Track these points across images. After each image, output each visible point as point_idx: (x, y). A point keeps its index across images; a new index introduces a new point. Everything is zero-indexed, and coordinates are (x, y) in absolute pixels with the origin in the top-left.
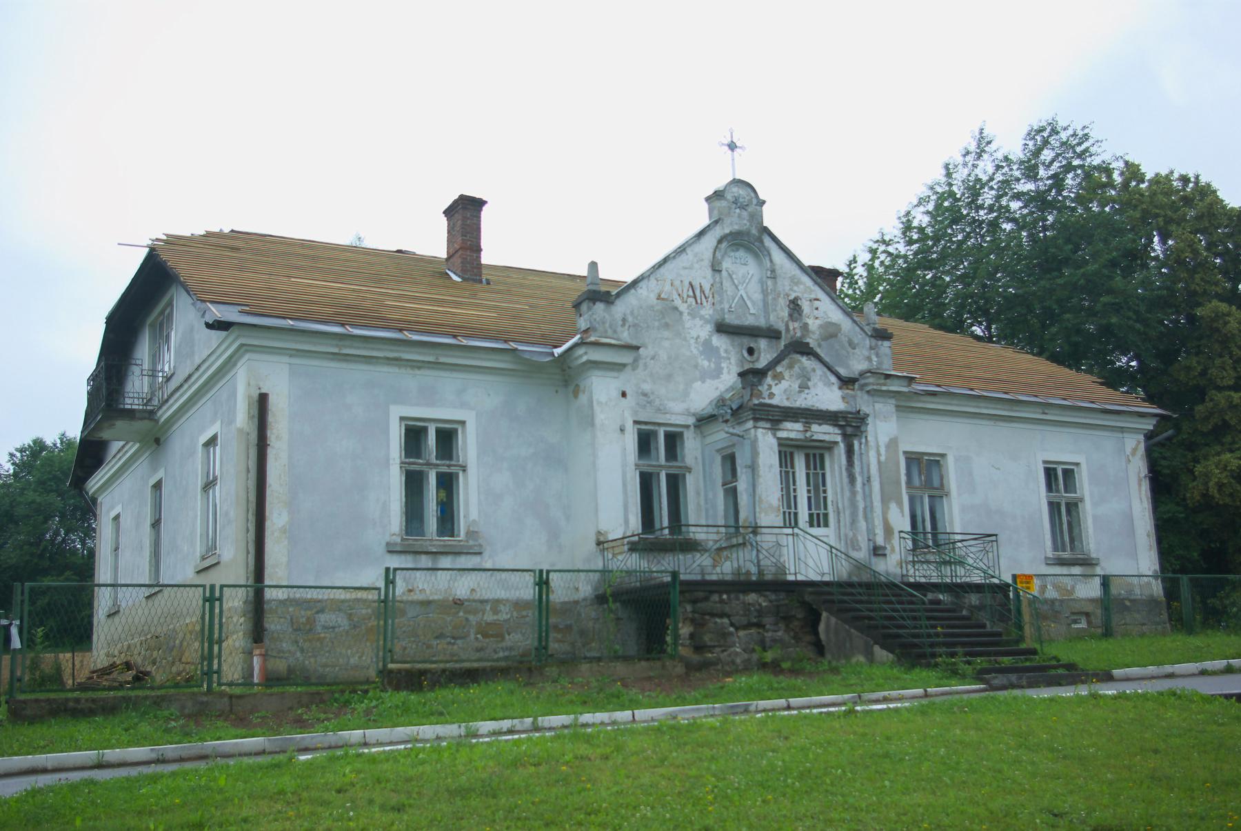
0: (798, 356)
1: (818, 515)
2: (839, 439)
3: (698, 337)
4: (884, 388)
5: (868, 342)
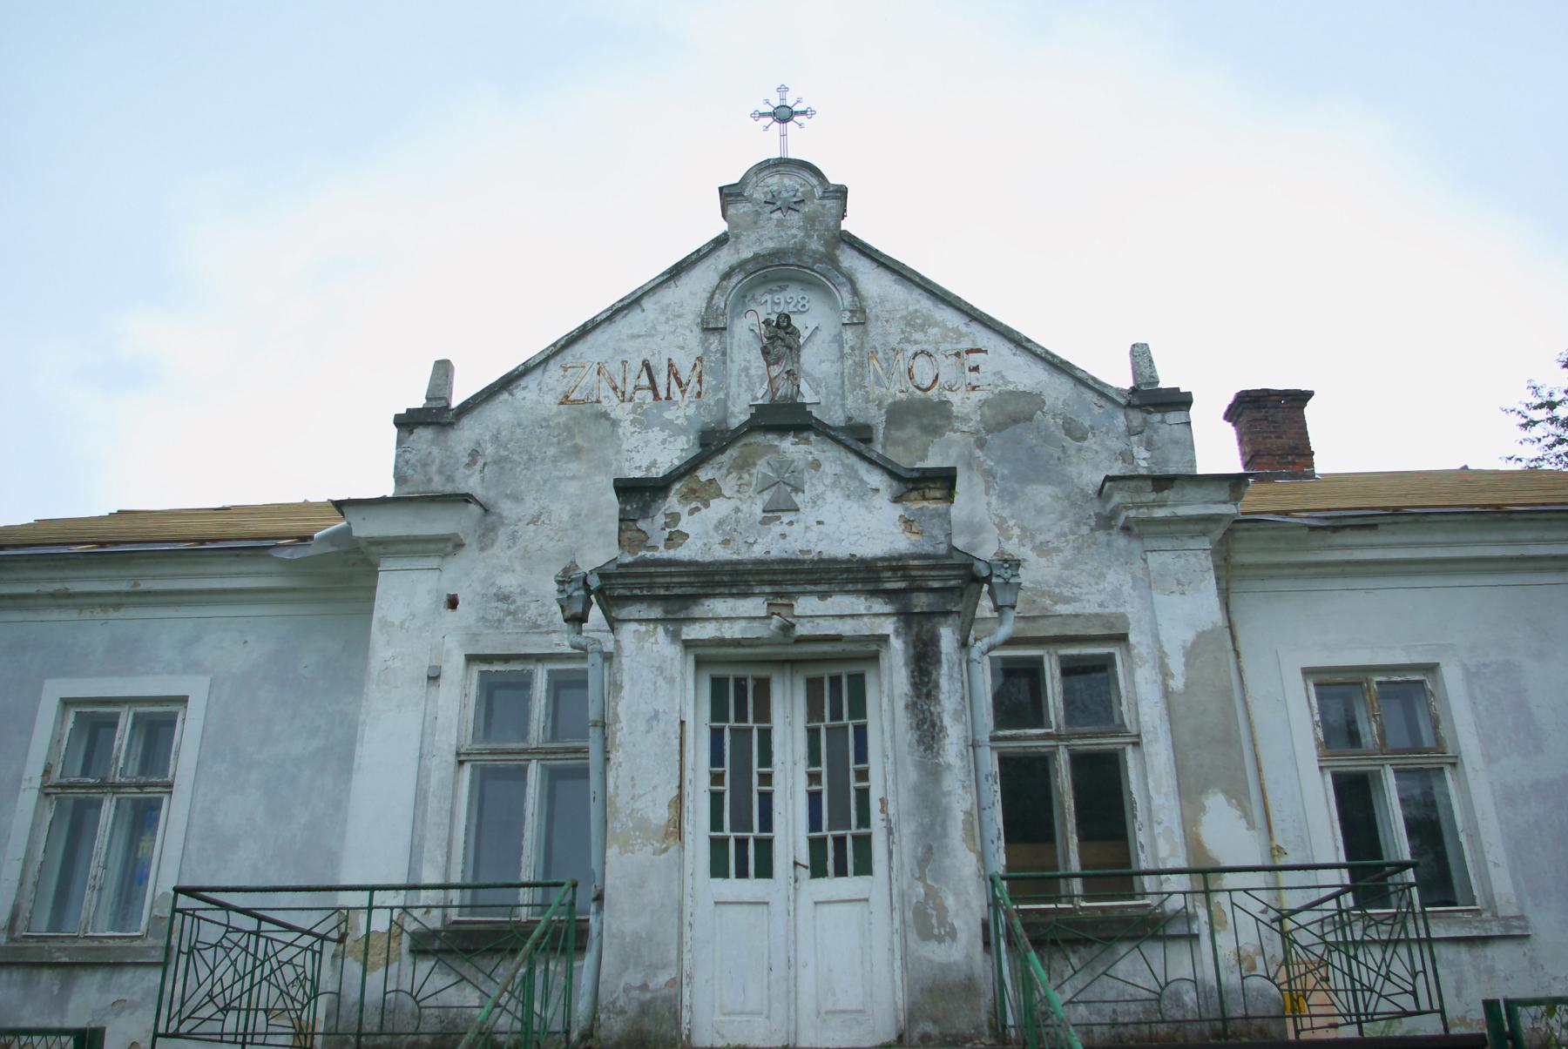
0: (772, 439)
1: (840, 842)
2: (888, 627)
5: (1120, 420)
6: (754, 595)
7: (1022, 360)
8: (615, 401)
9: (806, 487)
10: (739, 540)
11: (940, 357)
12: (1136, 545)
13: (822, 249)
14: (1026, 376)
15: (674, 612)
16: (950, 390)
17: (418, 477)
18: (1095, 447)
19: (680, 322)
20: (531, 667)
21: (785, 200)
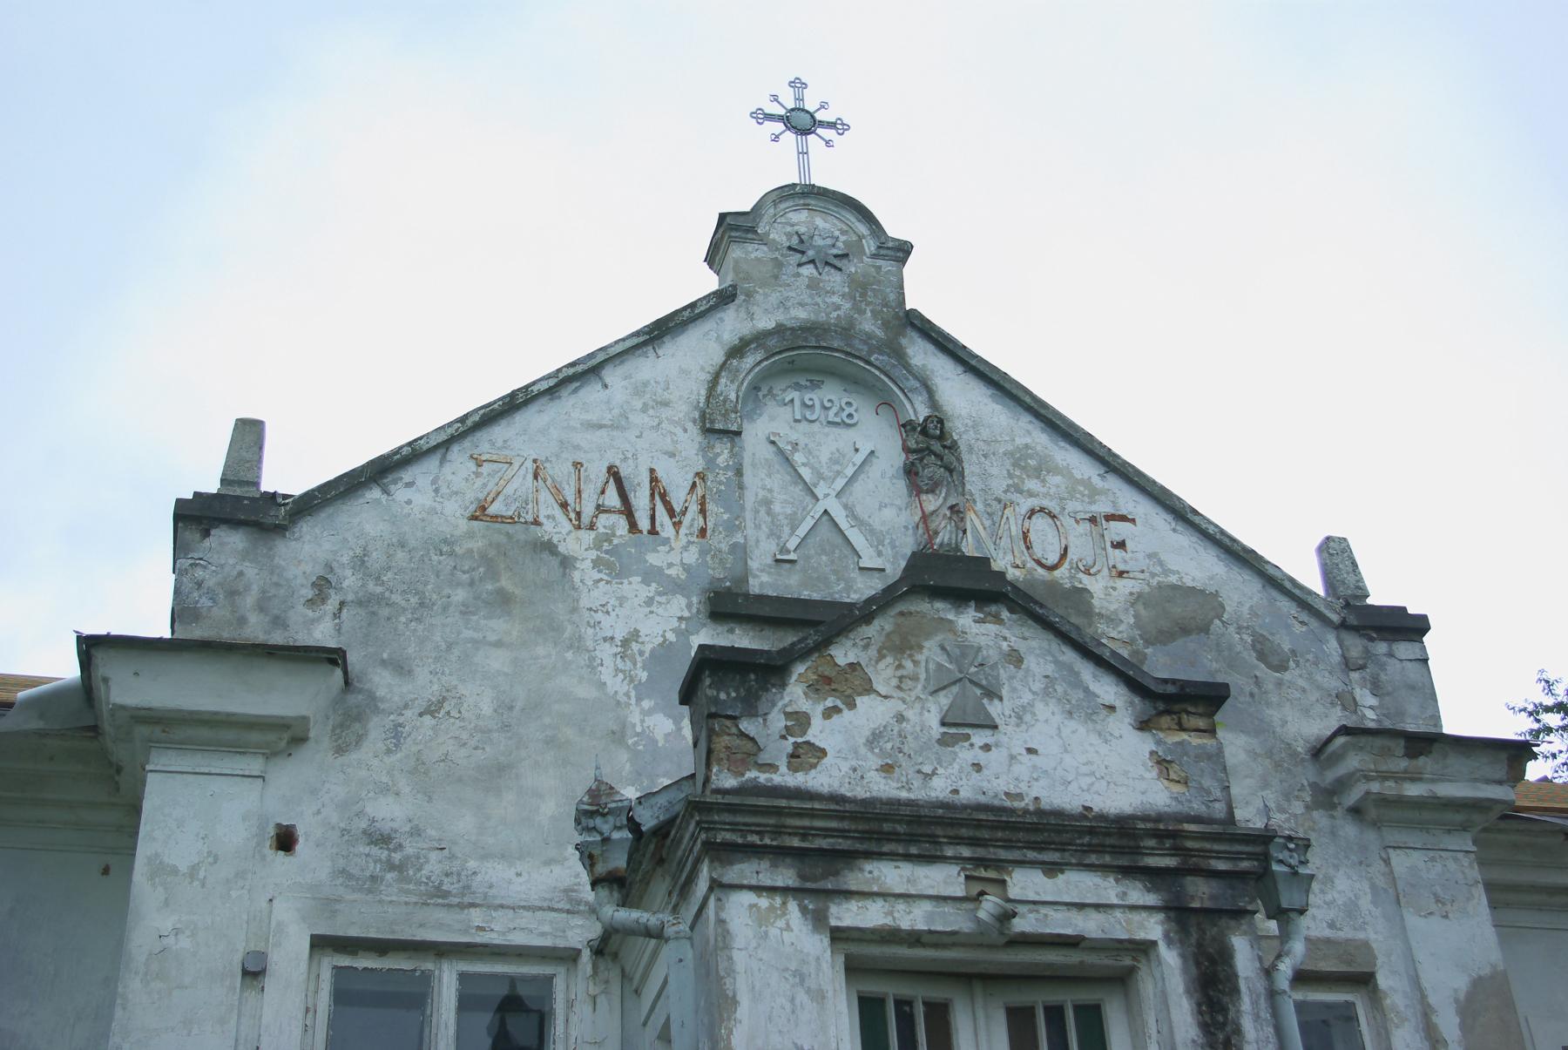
0: (942, 608)
2: (1153, 928)
3: (635, 635)
4: (1413, 790)
5: (1332, 645)
6: (943, 859)
7: (1184, 540)
8: (567, 526)
9: (1005, 692)
10: (907, 768)
11: (1067, 521)
12: (1371, 835)
13: (880, 333)
14: (1197, 567)
15: (815, 880)
16: (1087, 572)
17: (221, 612)
18: (1301, 682)
19: (666, 413)
20: (429, 966)
21: (819, 250)
